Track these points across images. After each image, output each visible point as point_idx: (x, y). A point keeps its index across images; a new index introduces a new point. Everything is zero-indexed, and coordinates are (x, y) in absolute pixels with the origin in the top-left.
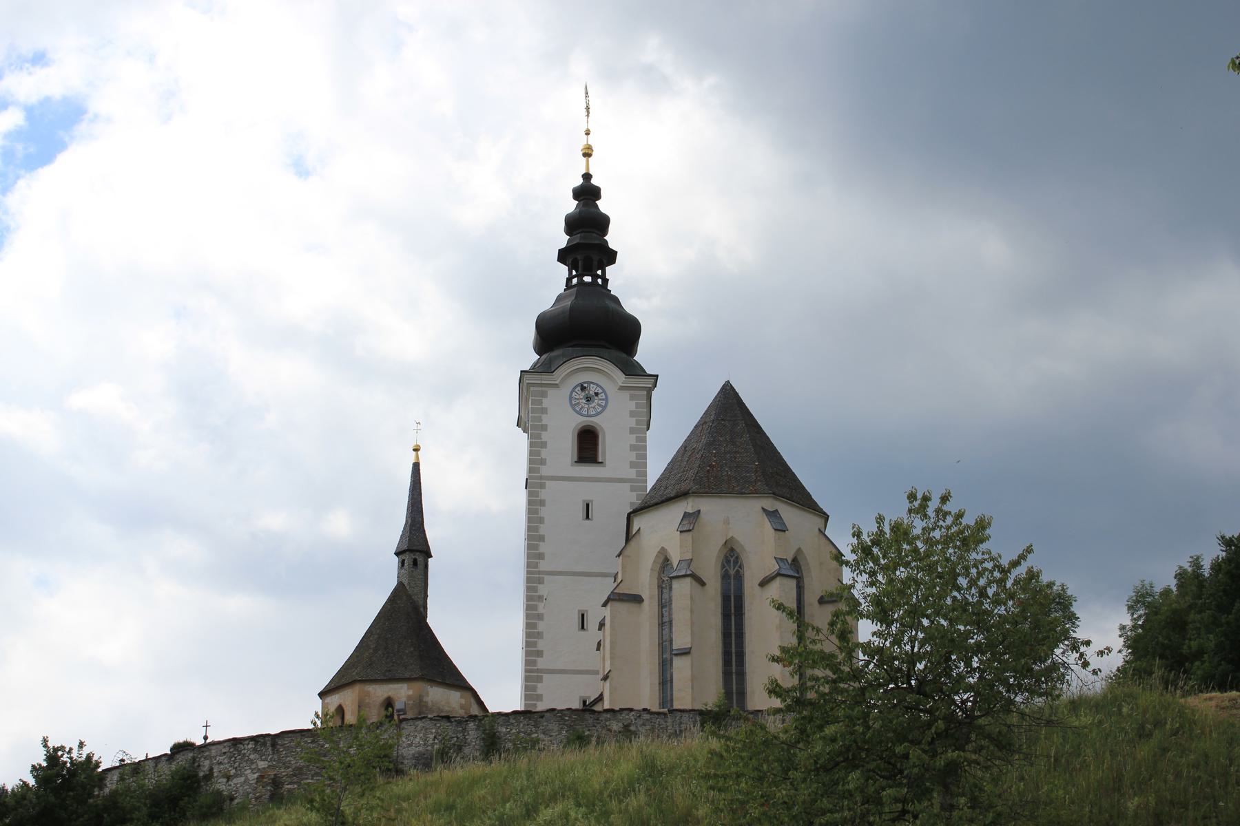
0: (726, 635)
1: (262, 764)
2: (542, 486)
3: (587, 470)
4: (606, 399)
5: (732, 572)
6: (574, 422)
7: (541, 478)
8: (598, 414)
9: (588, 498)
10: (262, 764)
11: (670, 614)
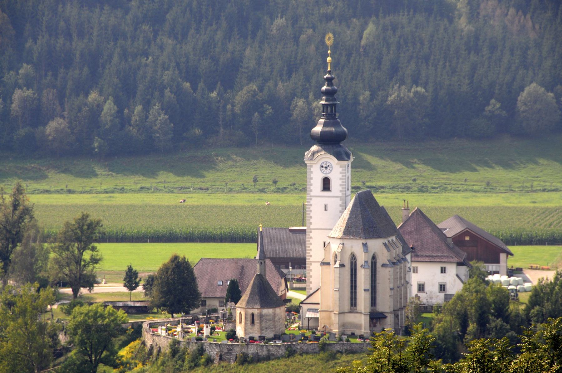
0: (352, 281)
1: (217, 350)
2: (311, 199)
3: (326, 193)
4: (332, 168)
5: (354, 262)
7: (311, 196)
8: (329, 173)
9: (326, 203)
10: (217, 350)
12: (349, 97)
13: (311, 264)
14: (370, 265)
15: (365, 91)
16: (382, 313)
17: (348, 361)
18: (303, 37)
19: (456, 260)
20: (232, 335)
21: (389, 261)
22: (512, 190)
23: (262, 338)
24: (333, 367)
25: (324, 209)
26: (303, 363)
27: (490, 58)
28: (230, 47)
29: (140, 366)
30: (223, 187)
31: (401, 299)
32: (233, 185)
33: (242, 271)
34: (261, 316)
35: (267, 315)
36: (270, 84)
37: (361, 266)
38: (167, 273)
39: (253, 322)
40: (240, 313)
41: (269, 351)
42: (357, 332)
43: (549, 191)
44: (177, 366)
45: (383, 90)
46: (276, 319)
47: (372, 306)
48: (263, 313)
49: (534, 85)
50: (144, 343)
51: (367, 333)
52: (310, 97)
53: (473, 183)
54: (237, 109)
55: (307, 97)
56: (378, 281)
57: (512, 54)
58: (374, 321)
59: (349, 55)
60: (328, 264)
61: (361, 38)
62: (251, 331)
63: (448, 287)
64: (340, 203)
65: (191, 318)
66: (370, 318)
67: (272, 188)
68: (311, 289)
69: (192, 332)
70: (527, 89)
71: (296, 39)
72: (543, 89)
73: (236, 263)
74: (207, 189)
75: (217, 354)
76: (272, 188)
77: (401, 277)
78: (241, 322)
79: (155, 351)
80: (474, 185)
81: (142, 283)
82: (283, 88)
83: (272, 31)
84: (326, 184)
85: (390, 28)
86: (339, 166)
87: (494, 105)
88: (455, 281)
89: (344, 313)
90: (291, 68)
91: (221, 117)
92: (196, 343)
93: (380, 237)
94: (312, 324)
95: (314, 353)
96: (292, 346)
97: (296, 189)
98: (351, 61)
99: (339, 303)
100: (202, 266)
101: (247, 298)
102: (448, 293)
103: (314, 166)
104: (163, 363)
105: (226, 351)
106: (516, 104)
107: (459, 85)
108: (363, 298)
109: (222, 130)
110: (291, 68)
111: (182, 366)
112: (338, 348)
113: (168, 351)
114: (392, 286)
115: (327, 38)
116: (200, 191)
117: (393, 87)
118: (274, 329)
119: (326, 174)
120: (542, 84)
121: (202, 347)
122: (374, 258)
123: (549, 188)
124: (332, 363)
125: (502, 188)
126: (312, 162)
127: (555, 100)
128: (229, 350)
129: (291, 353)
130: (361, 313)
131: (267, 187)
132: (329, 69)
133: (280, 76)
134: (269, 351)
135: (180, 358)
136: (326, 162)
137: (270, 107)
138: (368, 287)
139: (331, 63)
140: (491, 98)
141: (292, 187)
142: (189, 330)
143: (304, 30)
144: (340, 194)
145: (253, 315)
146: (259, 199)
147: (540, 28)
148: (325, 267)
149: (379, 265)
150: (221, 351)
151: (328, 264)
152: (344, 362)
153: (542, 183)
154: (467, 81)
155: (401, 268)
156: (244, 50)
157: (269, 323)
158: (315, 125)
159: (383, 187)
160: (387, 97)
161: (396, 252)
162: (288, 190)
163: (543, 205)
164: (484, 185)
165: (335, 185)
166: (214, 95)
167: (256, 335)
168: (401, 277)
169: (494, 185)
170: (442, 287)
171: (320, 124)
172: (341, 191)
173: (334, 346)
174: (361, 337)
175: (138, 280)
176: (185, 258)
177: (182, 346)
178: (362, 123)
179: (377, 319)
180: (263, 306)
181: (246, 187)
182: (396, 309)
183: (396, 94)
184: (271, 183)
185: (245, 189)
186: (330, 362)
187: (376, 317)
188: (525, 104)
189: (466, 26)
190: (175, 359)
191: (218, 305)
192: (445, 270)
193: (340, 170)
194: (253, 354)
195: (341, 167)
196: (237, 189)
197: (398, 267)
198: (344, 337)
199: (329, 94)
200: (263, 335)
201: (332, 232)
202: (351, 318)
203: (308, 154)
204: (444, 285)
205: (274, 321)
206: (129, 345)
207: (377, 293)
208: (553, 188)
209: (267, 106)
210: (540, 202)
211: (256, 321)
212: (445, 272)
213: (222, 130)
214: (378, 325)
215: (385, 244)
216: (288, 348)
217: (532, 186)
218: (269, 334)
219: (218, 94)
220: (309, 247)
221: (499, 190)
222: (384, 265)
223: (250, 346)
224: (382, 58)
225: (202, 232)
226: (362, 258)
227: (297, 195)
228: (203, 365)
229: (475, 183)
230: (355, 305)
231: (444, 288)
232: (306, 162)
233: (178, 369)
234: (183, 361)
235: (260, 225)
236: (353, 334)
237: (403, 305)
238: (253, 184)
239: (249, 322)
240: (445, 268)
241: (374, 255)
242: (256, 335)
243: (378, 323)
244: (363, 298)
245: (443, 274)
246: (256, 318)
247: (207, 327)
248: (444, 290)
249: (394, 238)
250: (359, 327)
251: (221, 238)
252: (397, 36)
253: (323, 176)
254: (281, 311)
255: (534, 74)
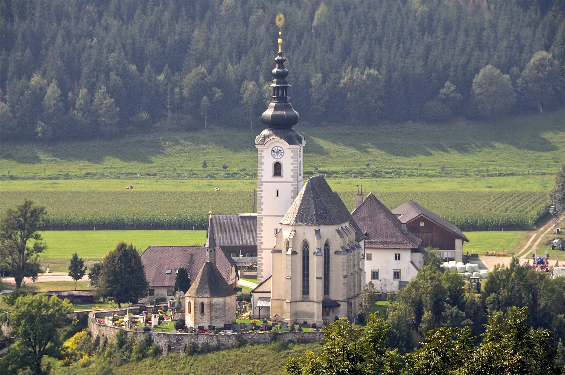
0: (304, 269)
1: (166, 341)
3: (278, 179)
4: (283, 152)
5: (306, 249)
6: (273, 161)
7: (262, 182)
9: (277, 189)
11: (302, 225)
12: (301, 79)
13: (262, 252)
14: (323, 252)
15: (317, 73)
16: (335, 302)
17: (300, 351)
18: (253, 18)
19: (411, 246)
20: (181, 325)
21: (342, 247)
22: (467, 175)
23: (212, 328)
24: (285, 357)
25: (275, 194)
26: (254, 353)
27: (445, 39)
28: (178, 27)
29: (86, 357)
30: (171, 172)
31: (355, 286)
32: (181, 170)
33: (191, 259)
34: (211, 305)
35: (217, 304)
36: (220, 66)
37: (314, 254)
38: (114, 262)
39: (202, 311)
40: (189, 302)
41: (219, 341)
42: (310, 321)
43: (505, 175)
44: (125, 357)
45: (335, 72)
46: (227, 308)
47: (325, 294)
48: (213, 302)
49: (489, 66)
50: (90, 334)
51: (320, 321)
52: (261, 80)
53: (427, 168)
54: (185, 93)
55: (257, 80)
56: (330, 269)
57: (467, 36)
58: (327, 309)
59: (300, 37)
60: (280, 251)
61: (312, 18)
62: (200, 320)
63: (402, 274)
64: (292, 188)
65: (139, 307)
66: (324, 307)
67: (222, 173)
68: (262, 277)
69: (140, 322)
70: (482, 71)
71: (246, 20)
72: (499, 71)
73: (185, 251)
74: (155, 175)
75: (165, 344)
76: (222, 173)
77: (354, 264)
78: (190, 312)
79: (101, 342)
80: (428, 170)
81: (88, 272)
82: (232, 71)
83: (221, 11)
84: (278, 169)
85: (342, 8)
86: (290, 151)
87: (449, 88)
88: (409, 268)
89: (296, 301)
90: (240, 51)
91: (169, 100)
92: (144, 333)
93: (333, 224)
94: (263, 313)
95: (266, 343)
96: (243, 336)
97: (247, 174)
98: (303, 42)
99: (292, 291)
100: (150, 253)
101: (197, 287)
102: (402, 280)
103: (265, 150)
104: (110, 354)
105: (175, 341)
106: (471, 86)
107: (413, 67)
108: (316, 286)
109: (170, 114)
110: (240, 51)
111: (129, 357)
112: (290, 337)
113: (115, 341)
114: (345, 274)
115: (277, 19)
116: (148, 177)
117: (346, 69)
118: (224, 319)
119: (277, 159)
120: (498, 66)
121: (150, 338)
122: (327, 244)
123: (505, 173)
124: (284, 353)
125: (457, 173)
126: (262, 146)
127: (510, 83)
128: (178, 340)
129: (242, 343)
130: (314, 301)
131: (216, 172)
132: (280, 51)
133: (230, 58)
134: (219, 341)
135: (127, 349)
136: (278, 147)
137: (219, 91)
138: (321, 274)
139: (282, 45)
140: (446, 81)
141: (242, 173)
142: (137, 320)
143: (254, 10)
144: (292, 180)
145: (202, 304)
146: (209, 185)
147: (495, 8)
148: (277, 254)
149: (332, 252)
150: (170, 342)
151: (280, 251)
152: (296, 351)
153: (498, 167)
154: (421, 63)
155: (354, 255)
156: (192, 31)
157: (219, 313)
158: (265, 109)
159: (336, 173)
160: (340, 79)
161: (349, 239)
162: (238, 175)
163: (498, 190)
164: (439, 169)
165: (287, 170)
166: (161, 77)
167: (206, 325)
168: (354, 264)
169: (449, 169)
170: (397, 275)
171: (271, 107)
172: (292, 177)
173: (285, 335)
174: (314, 326)
175: (83, 269)
176: (132, 246)
177: (130, 336)
178: (314, 106)
179: (329, 307)
180: (212, 296)
181: (195, 172)
182: (349, 297)
183: (349, 77)
184: (221, 168)
185: (194, 174)
186: (282, 352)
187: (329, 306)
188: (481, 86)
189: (419, 7)
190: (122, 350)
191: (166, 294)
192: (399, 257)
193: (292, 154)
194: (202, 344)
195: (292, 151)
196: (186, 174)
197: (352, 254)
198: (297, 326)
199: (280, 77)
200: (213, 325)
201: (284, 218)
202: (303, 307)
203: (258, 139)
204: (398, 273)
205: (225, 310)
206: (74, 336)
207: (330, 281)
208: (509, 172)
209: (217, 89)
210: (496, 187)
211: (206, 311)
212: (399, 259)
213: (170, 114)
214: (331, 313)
215: (338, 231)
216: (239, 337)
217: (488, 171)
218: (220, 324)
219: (166, 77)
220: (260, 234)
221: (454, 174)
222: (337, 252)
223: (199, 336)
224: (334, 39)
225: (150, 219)
226: (314, 245)
227: (248, 181)
228: (151, 355)
229: (430, 168)
230: (308, 294)
231: (398, 275)
232: (257, 147)
233: (125, 360)
234: (131, 352)
235: (210, 212)
236: (305, 323)
237: (356, 293)
238: (202, 169)
239: (198, 312)
240: (399, 255)
241: (327, 241)
242: (206, 325)
243: (331, 311)
244: (316, 286)
245: (397, 261)
246: (205, 307)
247: (155, 317)
248: (398, 278)
249: (347, 224)
250: (311, 315)
251: (170, 225)
252: (349, 17)
253: (274, 161)
254: (231, 300)
255: (489, 55)
